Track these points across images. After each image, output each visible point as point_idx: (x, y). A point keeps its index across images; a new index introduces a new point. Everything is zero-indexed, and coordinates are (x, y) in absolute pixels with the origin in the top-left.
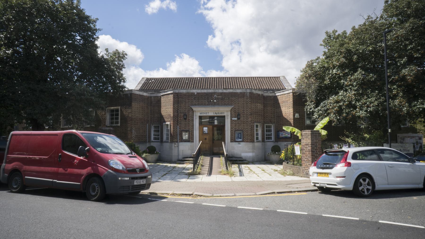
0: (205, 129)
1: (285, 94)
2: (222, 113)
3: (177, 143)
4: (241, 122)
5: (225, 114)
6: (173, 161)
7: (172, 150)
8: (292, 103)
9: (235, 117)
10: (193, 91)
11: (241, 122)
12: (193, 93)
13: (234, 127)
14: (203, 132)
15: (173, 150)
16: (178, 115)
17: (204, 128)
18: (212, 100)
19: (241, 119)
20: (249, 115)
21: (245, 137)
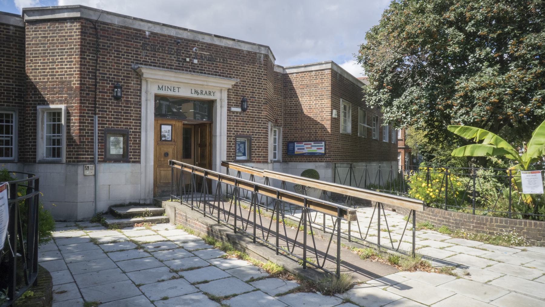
0: (166, 129)
1: (312, 71)
2: (210, 94)
3: (91, 166)
4: (248, 117)
5: (217, 96)
6: (80, 218)
7: (77, 184)
8: (330, 88)
9: (236, 106)
10: (140, 25)
11: (248, 117)
12: (140, 30)
13: (234, 129)
14: (161, 137)
15: (79, 186)
16: (96, 85)
17: (163, 126)
18: (188, 57)
19: (248, 112)
20: (264, 103)
21: (255, 152)
